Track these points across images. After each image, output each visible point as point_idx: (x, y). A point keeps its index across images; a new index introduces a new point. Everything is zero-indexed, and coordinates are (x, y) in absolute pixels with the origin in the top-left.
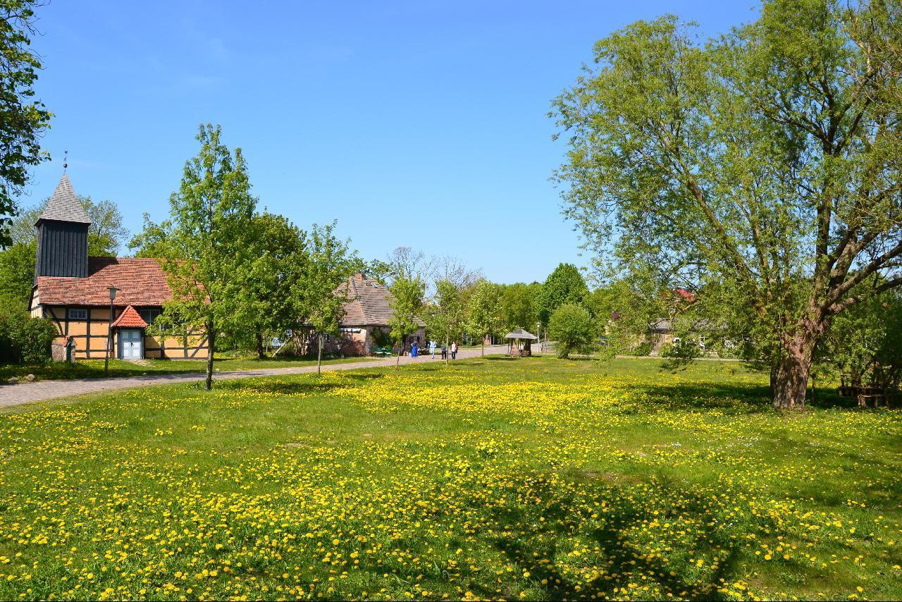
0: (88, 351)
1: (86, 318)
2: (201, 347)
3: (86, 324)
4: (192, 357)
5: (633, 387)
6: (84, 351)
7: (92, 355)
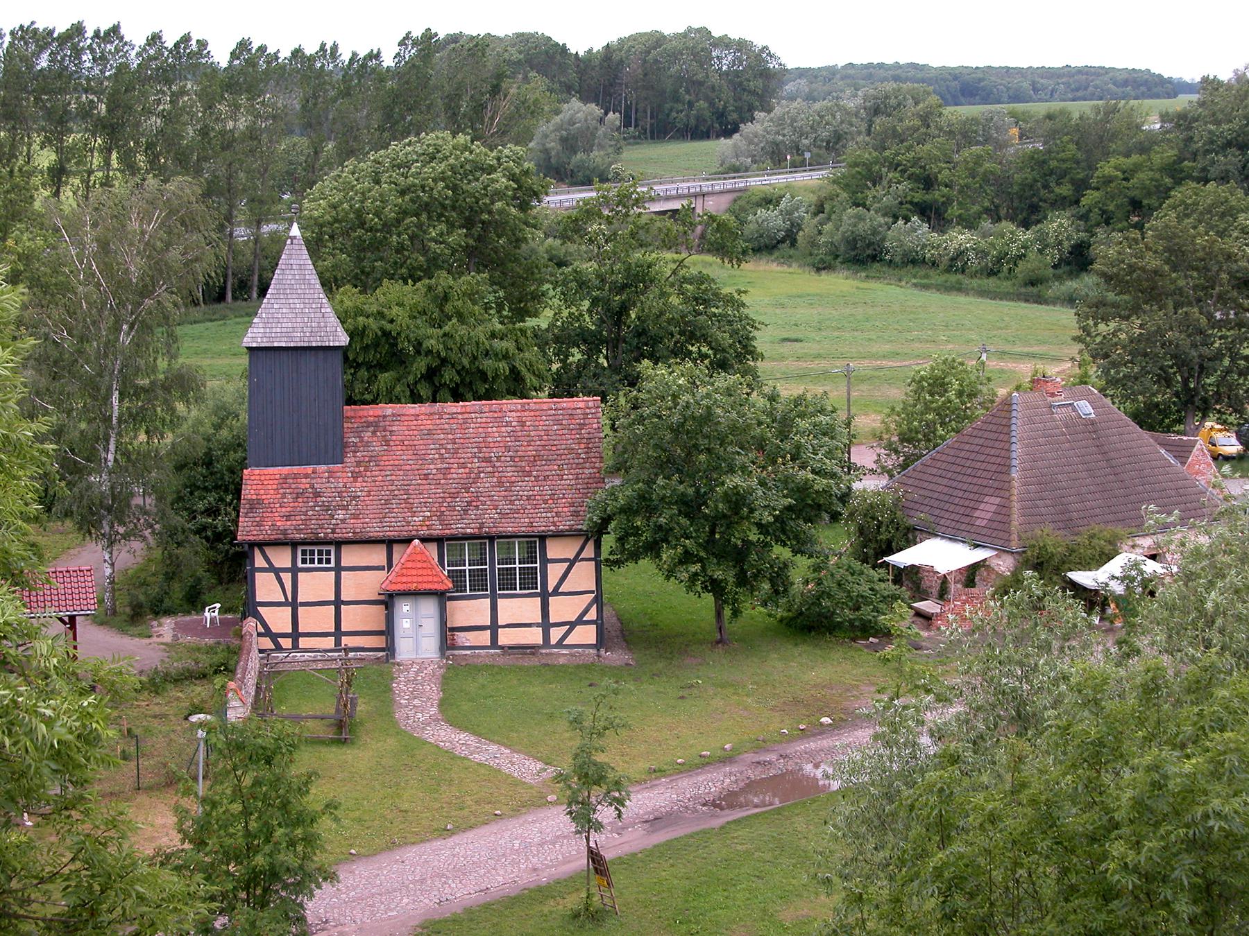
0: (338, 633)
1: (332, 565)
2: (580, 621)
3: (549, 565)
4: (560, 644)
5: (655, 771)
6: (538, 625)
7: (346, 641)
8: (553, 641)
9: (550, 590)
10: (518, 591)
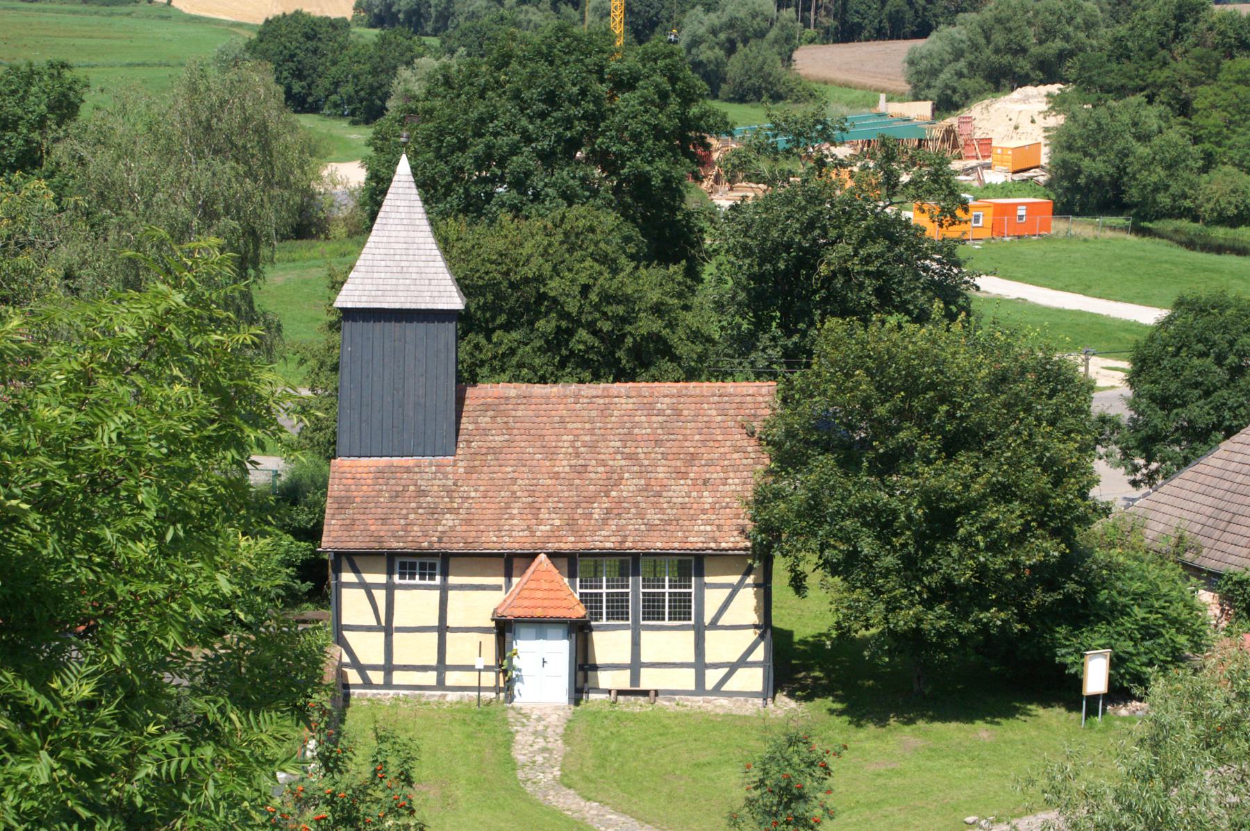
2: (743, 662)
4: (717, 690)
8: (709, 686)
9: (707, 620)
10: (667, 622)
